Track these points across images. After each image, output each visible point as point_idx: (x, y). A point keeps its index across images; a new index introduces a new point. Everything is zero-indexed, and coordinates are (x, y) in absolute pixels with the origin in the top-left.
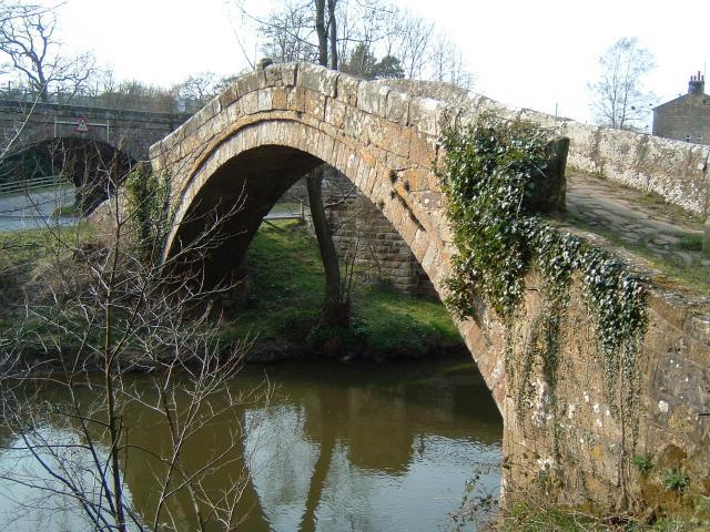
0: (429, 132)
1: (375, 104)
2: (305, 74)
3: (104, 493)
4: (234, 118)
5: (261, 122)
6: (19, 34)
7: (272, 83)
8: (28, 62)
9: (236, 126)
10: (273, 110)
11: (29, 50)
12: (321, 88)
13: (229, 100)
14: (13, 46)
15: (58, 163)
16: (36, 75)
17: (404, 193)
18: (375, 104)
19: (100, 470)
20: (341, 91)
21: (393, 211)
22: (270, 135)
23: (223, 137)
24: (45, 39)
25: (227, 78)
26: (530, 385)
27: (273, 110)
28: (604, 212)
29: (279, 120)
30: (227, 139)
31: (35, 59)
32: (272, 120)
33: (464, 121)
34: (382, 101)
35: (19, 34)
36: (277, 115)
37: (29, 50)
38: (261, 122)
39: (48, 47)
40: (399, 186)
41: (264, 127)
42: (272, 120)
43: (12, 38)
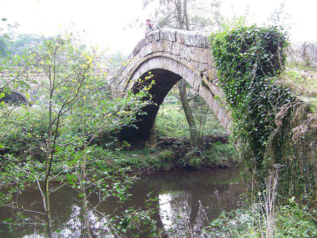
1: (191, 40)
2: (163, 33)
3: (56, 122)
5: (149, 59)
7: (151, 41)
12: (170, 38)
17: (206, 82)
18: (191, 40)
19: (58, 120)
20: (178, 38)
22: (154, 64)
23: (134, 69)
25: (148, 4)
26: (97, 230)
27: (153, 53)
29: (156, 57)
30: (137, 70)
32: (153, 58)
34: (194, 38)
36: (154, 55)
38: (149, 59)
40: (204, 78)
41: (150, 62)
42: (153, 58)
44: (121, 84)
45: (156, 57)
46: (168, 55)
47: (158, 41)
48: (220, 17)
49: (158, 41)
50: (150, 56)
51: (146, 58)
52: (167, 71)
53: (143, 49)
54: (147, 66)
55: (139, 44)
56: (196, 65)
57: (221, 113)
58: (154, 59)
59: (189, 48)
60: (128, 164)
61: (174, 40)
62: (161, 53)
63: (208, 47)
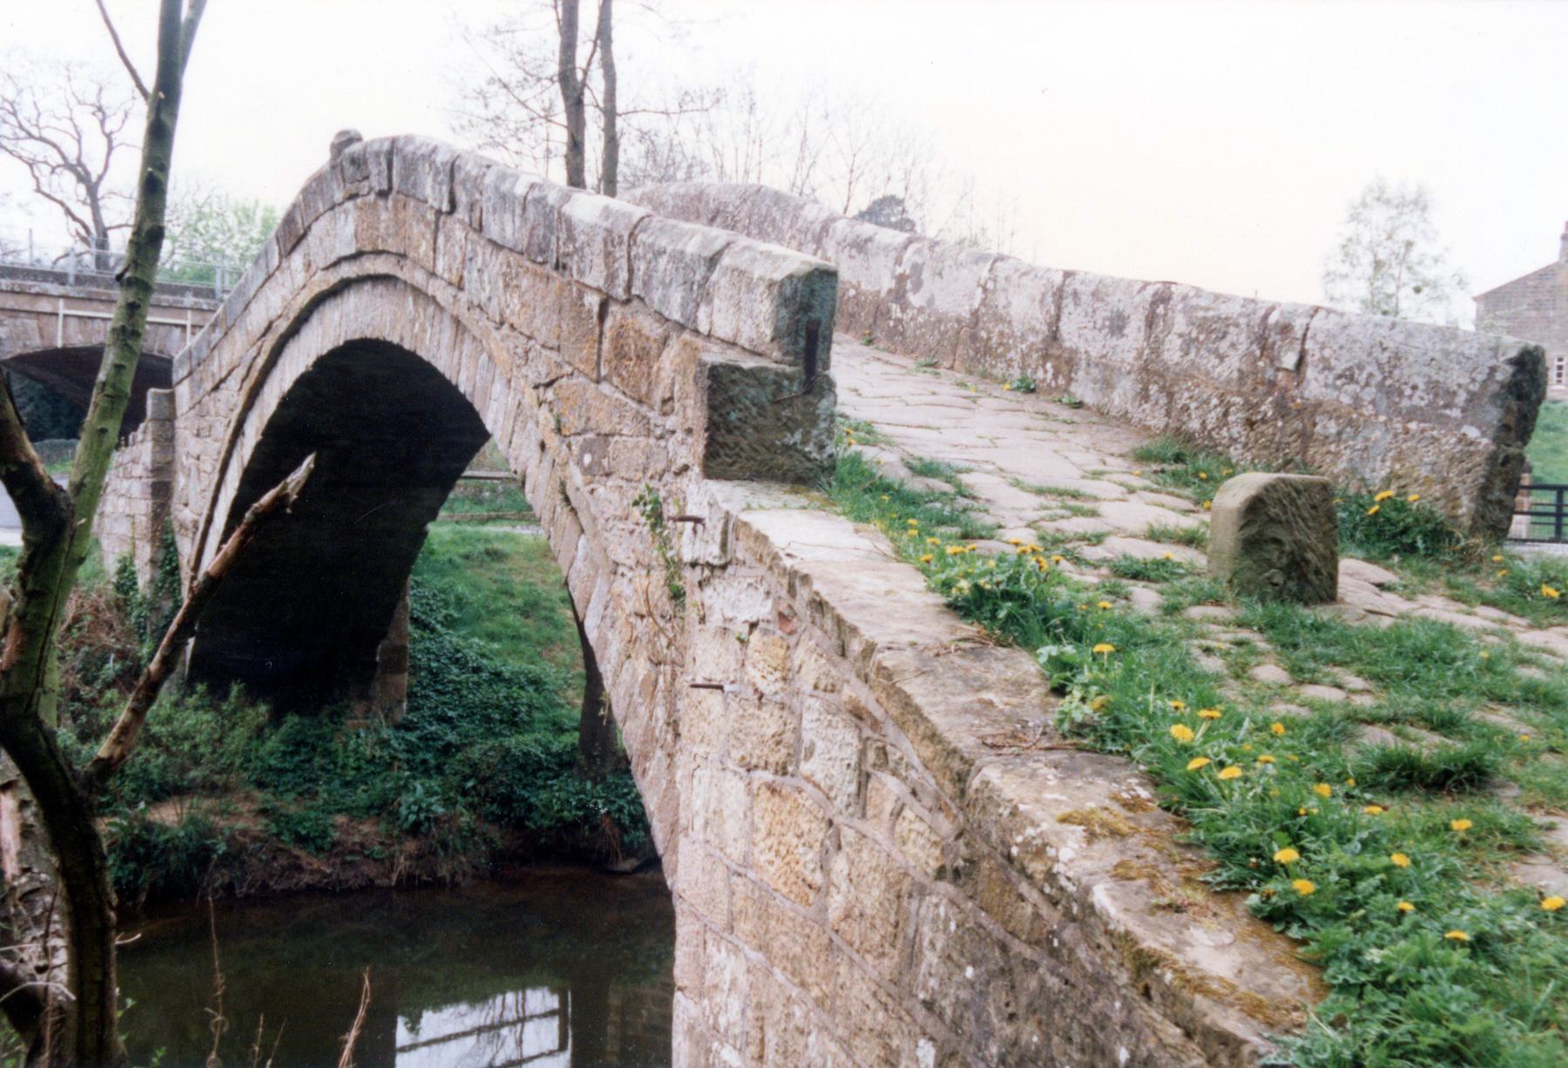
0: (588, 280)
2: (404, 158)
4: (300, 278)
6: (53, 122)
8: (68, 186)
9: (304, 299)
10: (358, 255)
11: (73, 160)
13: (292, 235)
14: (31, 148)
15: (1114, 592)
16: (85, 214)
21: (59, 630)
23: (282, 326)
24: (109, 136)
27: (358, 255)
28: (1177, 491)
31: (83, 177)
33: (1261, 959)
35: (53, 122)
37: (73, 160)
39: (115, 153)
41: (352, 301)
43: (35, 132)
44: (223, 394)
45: (376, 279)
46: (419, 278)
47: (383, 194)
48: (1056, 621)
49: (383, 194)
50: (348, 271)
51: (333, 278)
52: (412, 357)
53: (323, 222)
54: (337, 315)
55: (306, 192)
56: (520, 351)
57: (601, 608)
58: (368, 287)
59: (502, 256)
60: (608, 254)
61: (445, 207)
62: (393, 259)
63: (564, 267)
